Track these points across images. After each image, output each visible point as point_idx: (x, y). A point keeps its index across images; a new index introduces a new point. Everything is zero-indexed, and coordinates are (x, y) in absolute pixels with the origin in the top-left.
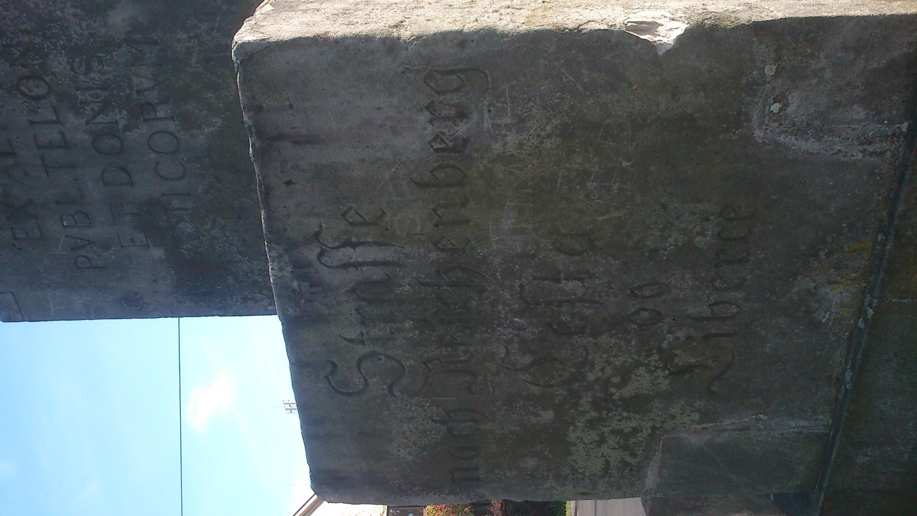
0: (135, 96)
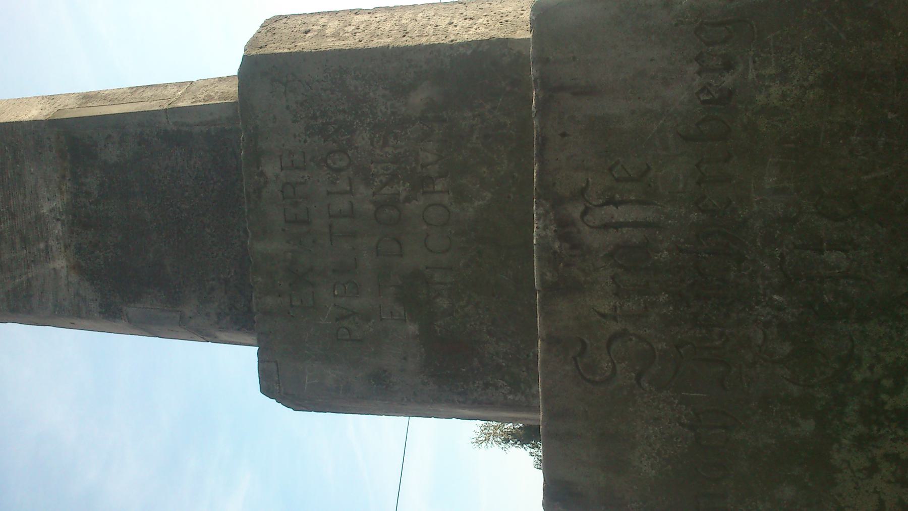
0: (419, 169)
